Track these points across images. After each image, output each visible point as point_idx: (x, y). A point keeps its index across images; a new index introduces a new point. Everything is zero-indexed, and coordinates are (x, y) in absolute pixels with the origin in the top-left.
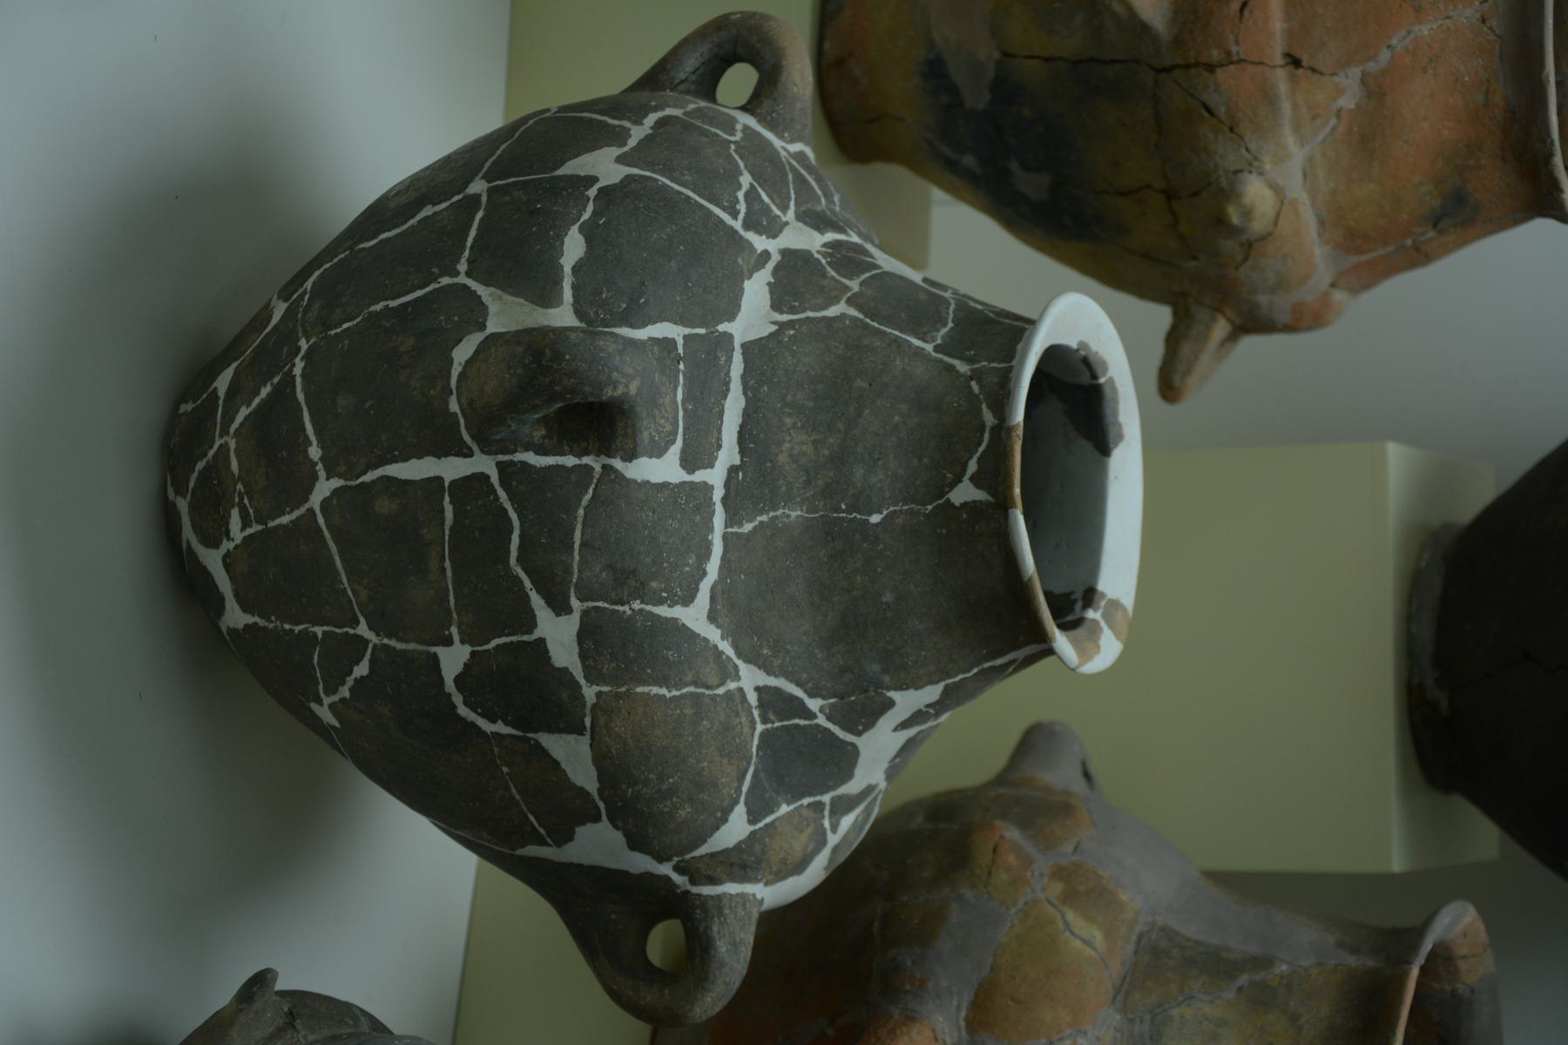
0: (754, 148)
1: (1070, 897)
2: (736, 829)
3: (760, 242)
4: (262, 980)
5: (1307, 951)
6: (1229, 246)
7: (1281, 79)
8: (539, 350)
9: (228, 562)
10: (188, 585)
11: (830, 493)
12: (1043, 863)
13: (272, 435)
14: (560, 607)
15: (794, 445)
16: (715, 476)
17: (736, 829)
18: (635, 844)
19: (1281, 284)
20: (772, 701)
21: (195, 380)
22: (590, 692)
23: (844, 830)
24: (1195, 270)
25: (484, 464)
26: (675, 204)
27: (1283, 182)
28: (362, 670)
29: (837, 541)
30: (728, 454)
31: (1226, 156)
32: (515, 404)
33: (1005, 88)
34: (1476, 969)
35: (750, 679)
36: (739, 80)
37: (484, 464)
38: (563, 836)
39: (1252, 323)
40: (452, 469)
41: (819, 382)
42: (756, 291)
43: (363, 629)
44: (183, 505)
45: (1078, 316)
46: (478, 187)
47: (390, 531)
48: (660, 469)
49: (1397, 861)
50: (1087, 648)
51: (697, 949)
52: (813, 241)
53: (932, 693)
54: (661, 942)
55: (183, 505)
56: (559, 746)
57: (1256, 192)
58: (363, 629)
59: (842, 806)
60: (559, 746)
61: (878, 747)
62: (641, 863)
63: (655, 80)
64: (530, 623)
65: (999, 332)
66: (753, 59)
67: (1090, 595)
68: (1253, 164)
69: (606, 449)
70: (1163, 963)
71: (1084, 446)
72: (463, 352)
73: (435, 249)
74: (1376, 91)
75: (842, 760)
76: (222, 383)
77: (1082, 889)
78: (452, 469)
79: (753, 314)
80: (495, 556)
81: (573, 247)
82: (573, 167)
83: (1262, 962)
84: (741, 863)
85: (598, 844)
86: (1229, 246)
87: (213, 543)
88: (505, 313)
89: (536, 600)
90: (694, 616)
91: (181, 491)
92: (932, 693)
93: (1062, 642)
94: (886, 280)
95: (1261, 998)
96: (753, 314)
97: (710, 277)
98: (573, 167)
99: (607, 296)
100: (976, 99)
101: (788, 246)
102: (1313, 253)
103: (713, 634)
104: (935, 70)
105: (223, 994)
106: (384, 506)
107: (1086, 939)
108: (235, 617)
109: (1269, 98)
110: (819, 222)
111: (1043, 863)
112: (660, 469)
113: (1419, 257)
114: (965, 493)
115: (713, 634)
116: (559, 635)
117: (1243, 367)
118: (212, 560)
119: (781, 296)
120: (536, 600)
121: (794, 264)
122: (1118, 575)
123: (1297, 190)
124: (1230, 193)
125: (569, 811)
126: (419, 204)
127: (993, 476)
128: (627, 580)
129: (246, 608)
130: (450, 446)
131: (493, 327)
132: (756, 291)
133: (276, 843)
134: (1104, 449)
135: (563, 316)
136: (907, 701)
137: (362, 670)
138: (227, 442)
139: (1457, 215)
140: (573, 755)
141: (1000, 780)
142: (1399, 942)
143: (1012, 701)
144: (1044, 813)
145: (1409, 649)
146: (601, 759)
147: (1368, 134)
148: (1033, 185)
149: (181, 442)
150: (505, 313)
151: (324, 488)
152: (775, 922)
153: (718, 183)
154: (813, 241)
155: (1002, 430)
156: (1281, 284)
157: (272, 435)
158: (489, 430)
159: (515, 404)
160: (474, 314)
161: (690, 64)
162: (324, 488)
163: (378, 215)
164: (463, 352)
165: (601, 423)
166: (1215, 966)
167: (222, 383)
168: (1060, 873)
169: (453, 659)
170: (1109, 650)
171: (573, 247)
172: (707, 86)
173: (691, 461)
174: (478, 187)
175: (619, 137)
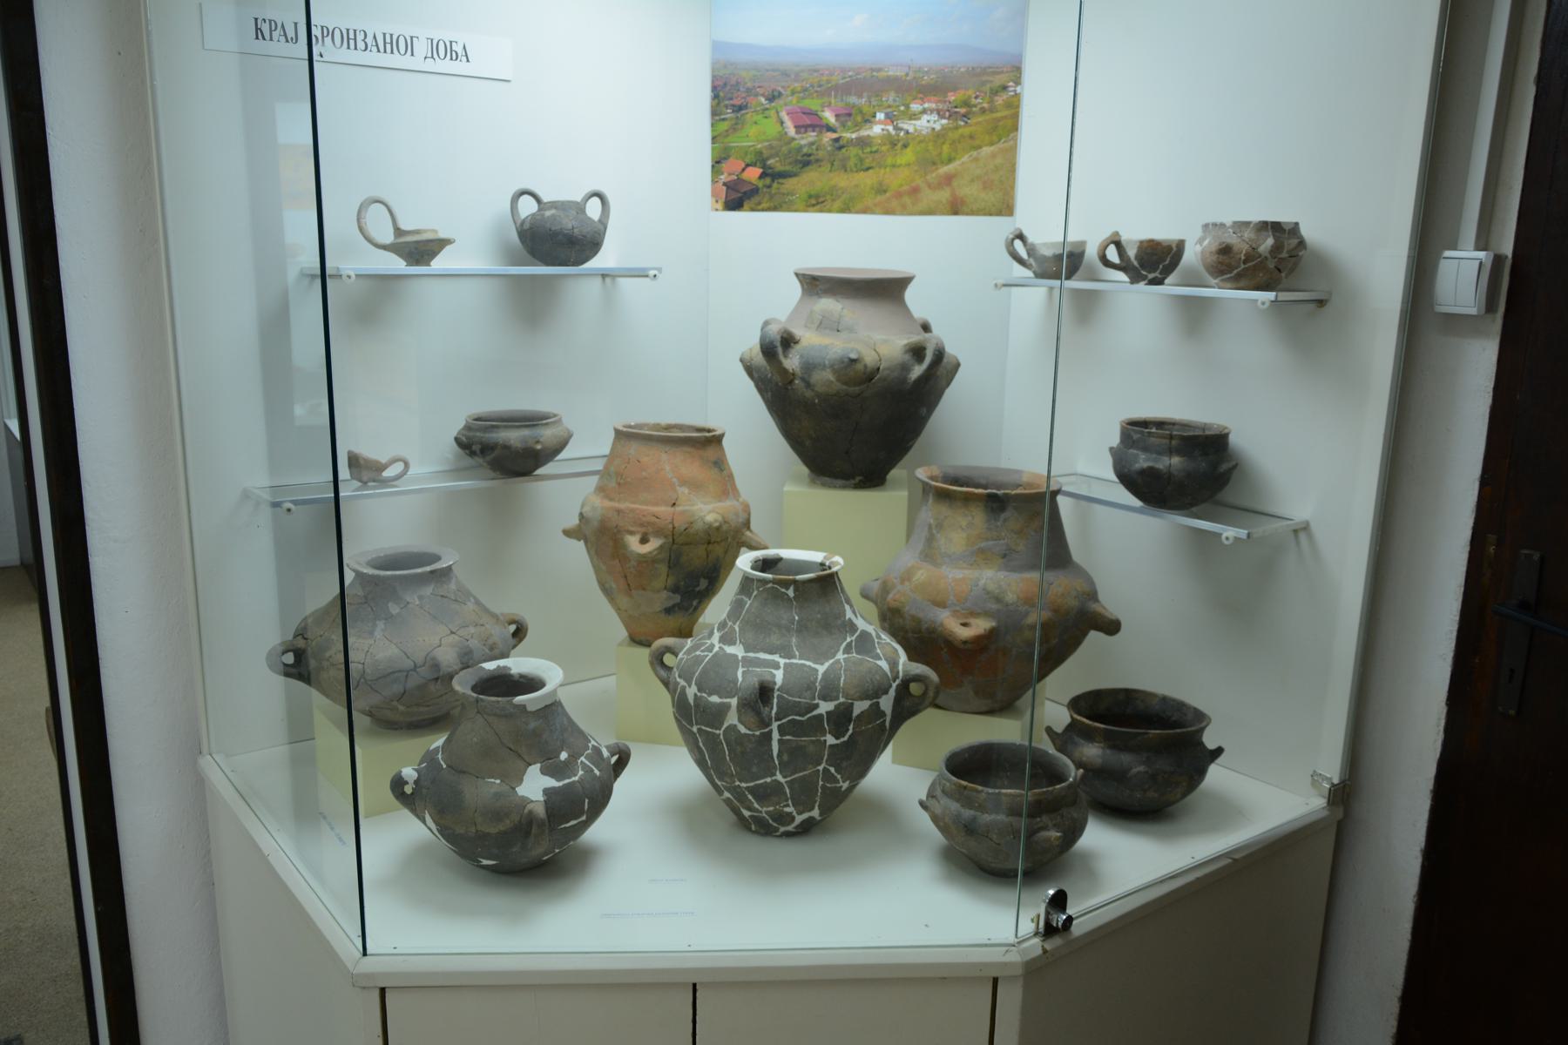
0: (689, 652)
1: (909, 580)
2: (883, 664)
3: (716, 649)
4: (922, 804)
5: (930, 512)
6: (725, 527)
7: (678, 509)
8: (747, 706)
9: (800, 813)
10: (806, 829)
11: (788, 630)
12: (899, 587)
13: (763, 794)
14: (817, 706)
15: (775, 639)
16: (782, 661)
17: (883, 664)
18: (886, 692)
19: (737, 514)
20: (848, 650)
21: (744, 824)
22: (842, 700)
23: (886, 638)
24: (732, 537)
25: (775, 725)
26: (704, 672)
27: (707, 511)
28: (832, 770)
29: (802, 628)
30: (776, 658)
31: (699, 526)
32: (758, 713)
33: (675, 590)
34: (935, 471)
35: (840, 656)
36: (668, 659)
37: (775, 725)
38: (883, 714)
39: (747, 524)
40: (776, 736)
41: (757, 631)
42: (730, 650)
43: (821, 768)
44: (782, 829)
45: (745, 561)
46: (695, 729)
47: (795, 757)
48: (779, 676)
49: (905, 493)
50: (837, 563)
51: (918, 678)
52: (717, 635)
53: (847, 607)
54: (915, 688)
55: (782, 829)
56: (856, 712)
57: (710, 518)
58: (821, 768)
59: (879, 637)
60: (856, 712)
61: (861, 624)
62: (892, 692)
63: (666, 684)
64: (821, 715)
65: (747, 583)
66: (662, 654)
67: (822, 564)
68: (702, 518)
69: (772, 690)
70: (929, 554)
71: (780, 565)
72: (743, 730)
73: (712, 741)
74: (683, 483)
75: (865, 634)
76: (746, 813)
77: (906, 577)
78: (776, 736)
79: (737, 650)
80: (802, 725)
81: (715, 699)
82: (691, 701)
83: (930, 527)
84: (893, 664)
85: (886, 703)
86: (725, 527)
87: (793, 819)
88: (732, 719)
89: (815, 713)
90: (821, 669)
91: (777, 830)
92: (847, 607)
93: (834, 569)
94: (729, 616)
95: (940, 526)
96: (737, 650)
97: (723, 663)
98: (691, 701)
99: (727, 689)
100: (677, 598)
101: (720, 635)
102: (729, 504)
103: (827, 665)
104: (668, 611)
105: (925, 818)
106: (785, 757)
107: (921, 575)
108: (815, 813)
109: (683, 512)
110: (711, 634)
111: (899, 587)
112: (779, 676)
113: (731, 476)
114: (791, 593)
115: (827, 665)
116: (825, 707)
117: (759, 527)
118: (799, 819)
119: (732, 643)
120: (815, 713)
121: (723, 640)
122: (816, 556)
123: (710, 507)
124: (710, 526)
125: (876, 711)
126: (698, 748)
127: (786, 584)
128: (810, 687)
129: (812, 809)
130: (768, 736)
131: (735, 721)
132: (730, 650)
133: (881, 813)
134: (780, 559)
135: (734, 702)
136: (849, 614)
137: (832, 770)
138: (764, 810)
139: (720, 464)
140: (860, 707)
141: (875, 603)
142: (926, 488)
143: (851, 585)
144: (886, 588)
145: (844, 487)
146: (861, 699)
147: (695, 486)
148: (703, 584)
149: (763, 828)
150: (732, 719)
151: (779, 777)
152: (911, 658)
153: (698, 660)
154: (717, 635)
155: (774, 581)
156: (737, 514)
157: (763, 794)
158: (765, 723)
159: (758, 713)
160: (732, 728)
161: (663, 673)
162: (779, 777)
163: (701, 763)
164: (743, 730)
165: (765, 691)
166: (930, 539)
167: (746, 813)
168: (902, 582)
169: (830, 740)
170: (838, 559)
171: (715, 699)
172: (669, 669)
173: (777, 666)
174: (695, 729)
175: (684, 688)
